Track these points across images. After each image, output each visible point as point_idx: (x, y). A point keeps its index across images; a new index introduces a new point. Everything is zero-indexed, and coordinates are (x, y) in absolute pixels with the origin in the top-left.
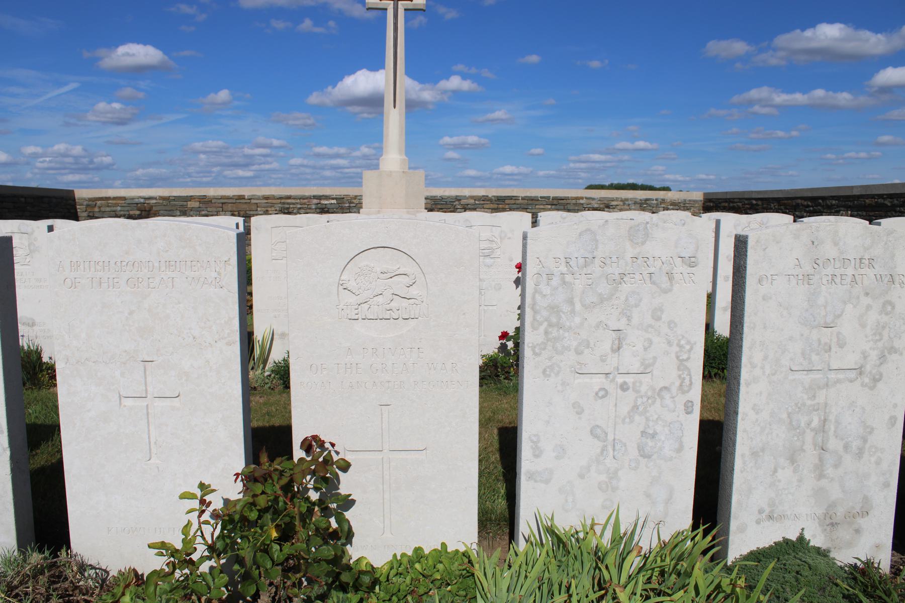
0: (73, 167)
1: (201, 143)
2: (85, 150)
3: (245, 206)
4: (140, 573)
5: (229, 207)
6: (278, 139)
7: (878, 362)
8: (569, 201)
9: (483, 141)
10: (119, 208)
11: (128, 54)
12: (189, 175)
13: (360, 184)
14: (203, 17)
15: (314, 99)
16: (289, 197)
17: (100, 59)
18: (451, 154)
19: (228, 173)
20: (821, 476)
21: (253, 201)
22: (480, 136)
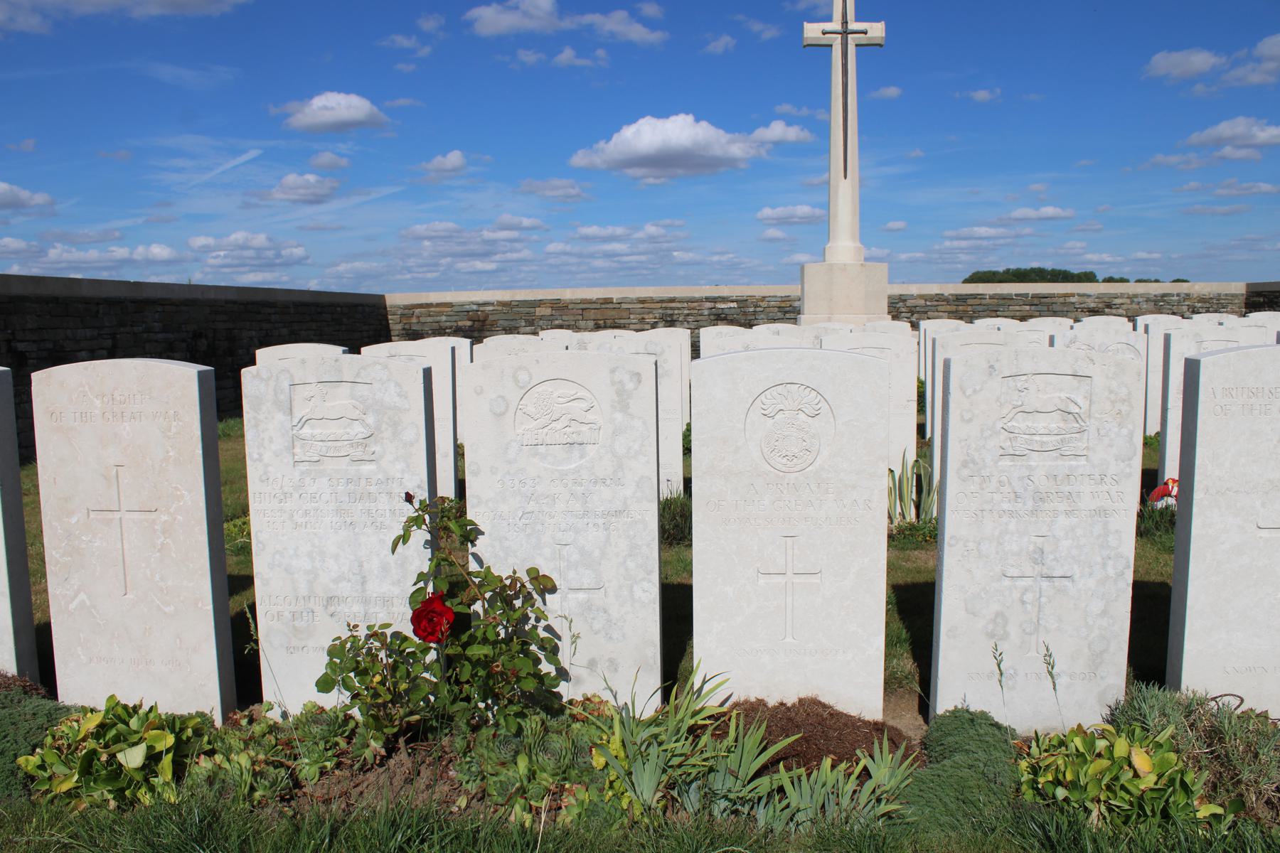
1: (425, 226)
2: (270, 239)
3: (613, 313)
5: (592, 314)
6: (529, 217)
8: (1054, 300)
10: (444, 318)
11: (325, 108)
12: (409, 270)
14: (425, 51)
15: (580, 159)
16: (672, 300)
17: (287, 116)
18: (773, 232)
19: (462, 265)
21: (624, 306)
22: (814, 206)
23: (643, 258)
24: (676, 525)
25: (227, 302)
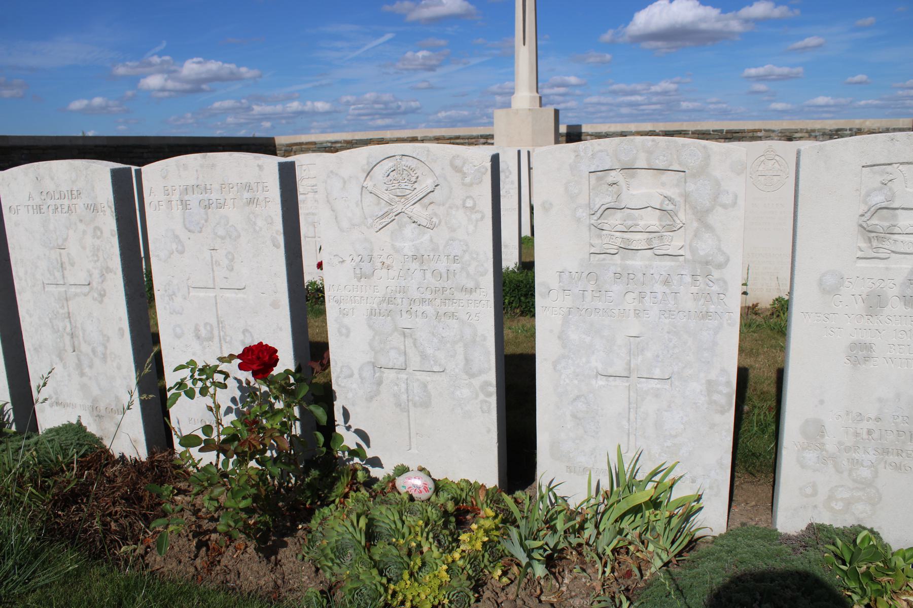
0: (384, 112)
4: (472, 482)
7: (100, 280)
9: (800, 69)
13: (491, 124)
20: (82, 374)
23: (658, 107)
24: (516, 293)
25: (96, 146)
